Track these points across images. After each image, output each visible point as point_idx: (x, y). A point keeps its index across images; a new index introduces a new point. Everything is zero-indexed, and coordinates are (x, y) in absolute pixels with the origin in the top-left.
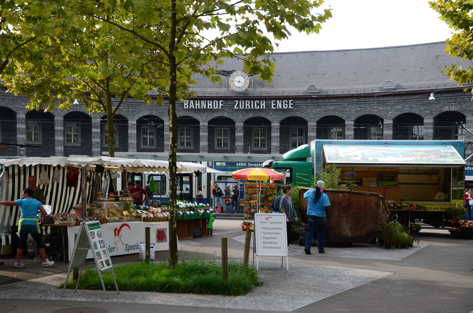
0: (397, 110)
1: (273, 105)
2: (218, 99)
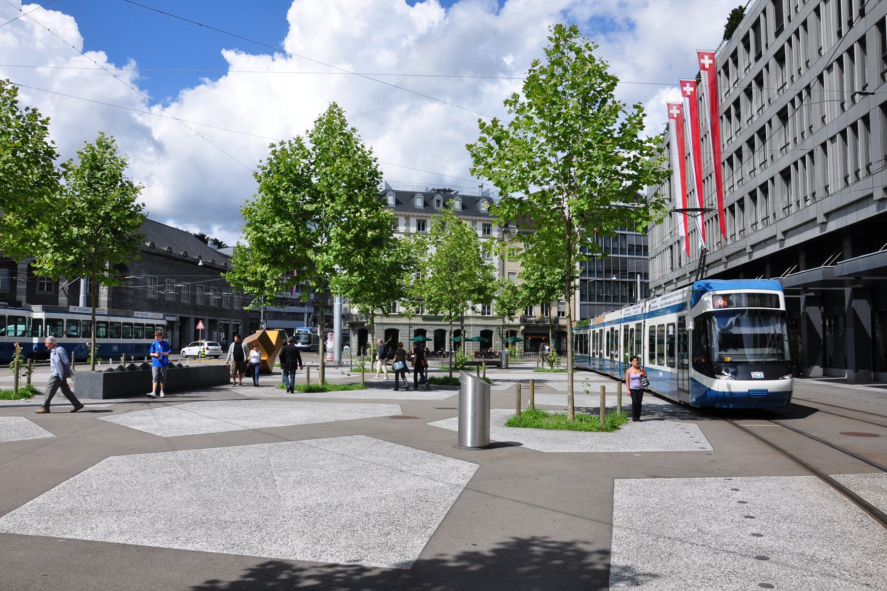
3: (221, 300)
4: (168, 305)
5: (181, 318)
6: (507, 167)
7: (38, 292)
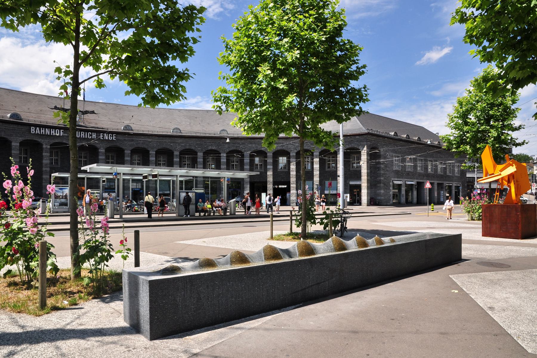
0: (182, 146)
1: (101, 136)
2: (60, 128)
3: (445, 168)
4: (408, 174)
5: (418, 183)
6: (305, 17)
7: (327, 169)
